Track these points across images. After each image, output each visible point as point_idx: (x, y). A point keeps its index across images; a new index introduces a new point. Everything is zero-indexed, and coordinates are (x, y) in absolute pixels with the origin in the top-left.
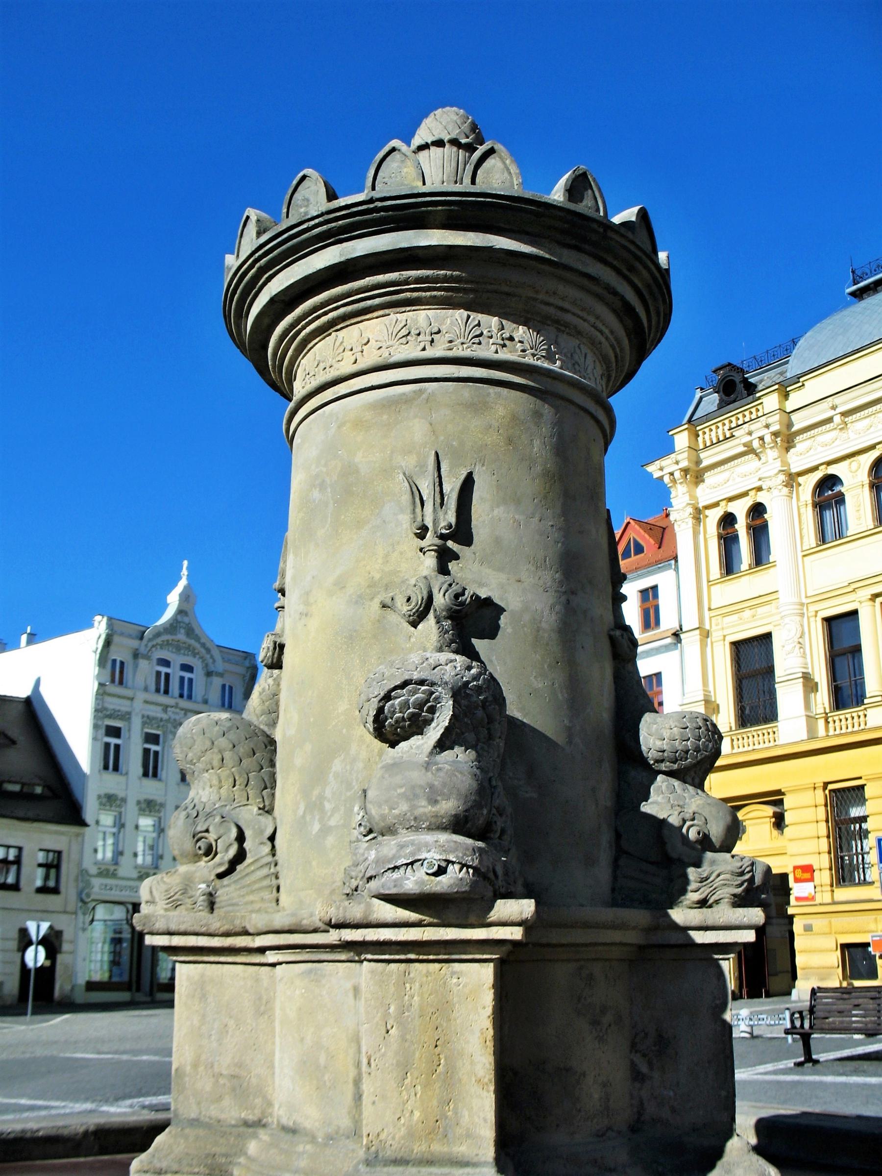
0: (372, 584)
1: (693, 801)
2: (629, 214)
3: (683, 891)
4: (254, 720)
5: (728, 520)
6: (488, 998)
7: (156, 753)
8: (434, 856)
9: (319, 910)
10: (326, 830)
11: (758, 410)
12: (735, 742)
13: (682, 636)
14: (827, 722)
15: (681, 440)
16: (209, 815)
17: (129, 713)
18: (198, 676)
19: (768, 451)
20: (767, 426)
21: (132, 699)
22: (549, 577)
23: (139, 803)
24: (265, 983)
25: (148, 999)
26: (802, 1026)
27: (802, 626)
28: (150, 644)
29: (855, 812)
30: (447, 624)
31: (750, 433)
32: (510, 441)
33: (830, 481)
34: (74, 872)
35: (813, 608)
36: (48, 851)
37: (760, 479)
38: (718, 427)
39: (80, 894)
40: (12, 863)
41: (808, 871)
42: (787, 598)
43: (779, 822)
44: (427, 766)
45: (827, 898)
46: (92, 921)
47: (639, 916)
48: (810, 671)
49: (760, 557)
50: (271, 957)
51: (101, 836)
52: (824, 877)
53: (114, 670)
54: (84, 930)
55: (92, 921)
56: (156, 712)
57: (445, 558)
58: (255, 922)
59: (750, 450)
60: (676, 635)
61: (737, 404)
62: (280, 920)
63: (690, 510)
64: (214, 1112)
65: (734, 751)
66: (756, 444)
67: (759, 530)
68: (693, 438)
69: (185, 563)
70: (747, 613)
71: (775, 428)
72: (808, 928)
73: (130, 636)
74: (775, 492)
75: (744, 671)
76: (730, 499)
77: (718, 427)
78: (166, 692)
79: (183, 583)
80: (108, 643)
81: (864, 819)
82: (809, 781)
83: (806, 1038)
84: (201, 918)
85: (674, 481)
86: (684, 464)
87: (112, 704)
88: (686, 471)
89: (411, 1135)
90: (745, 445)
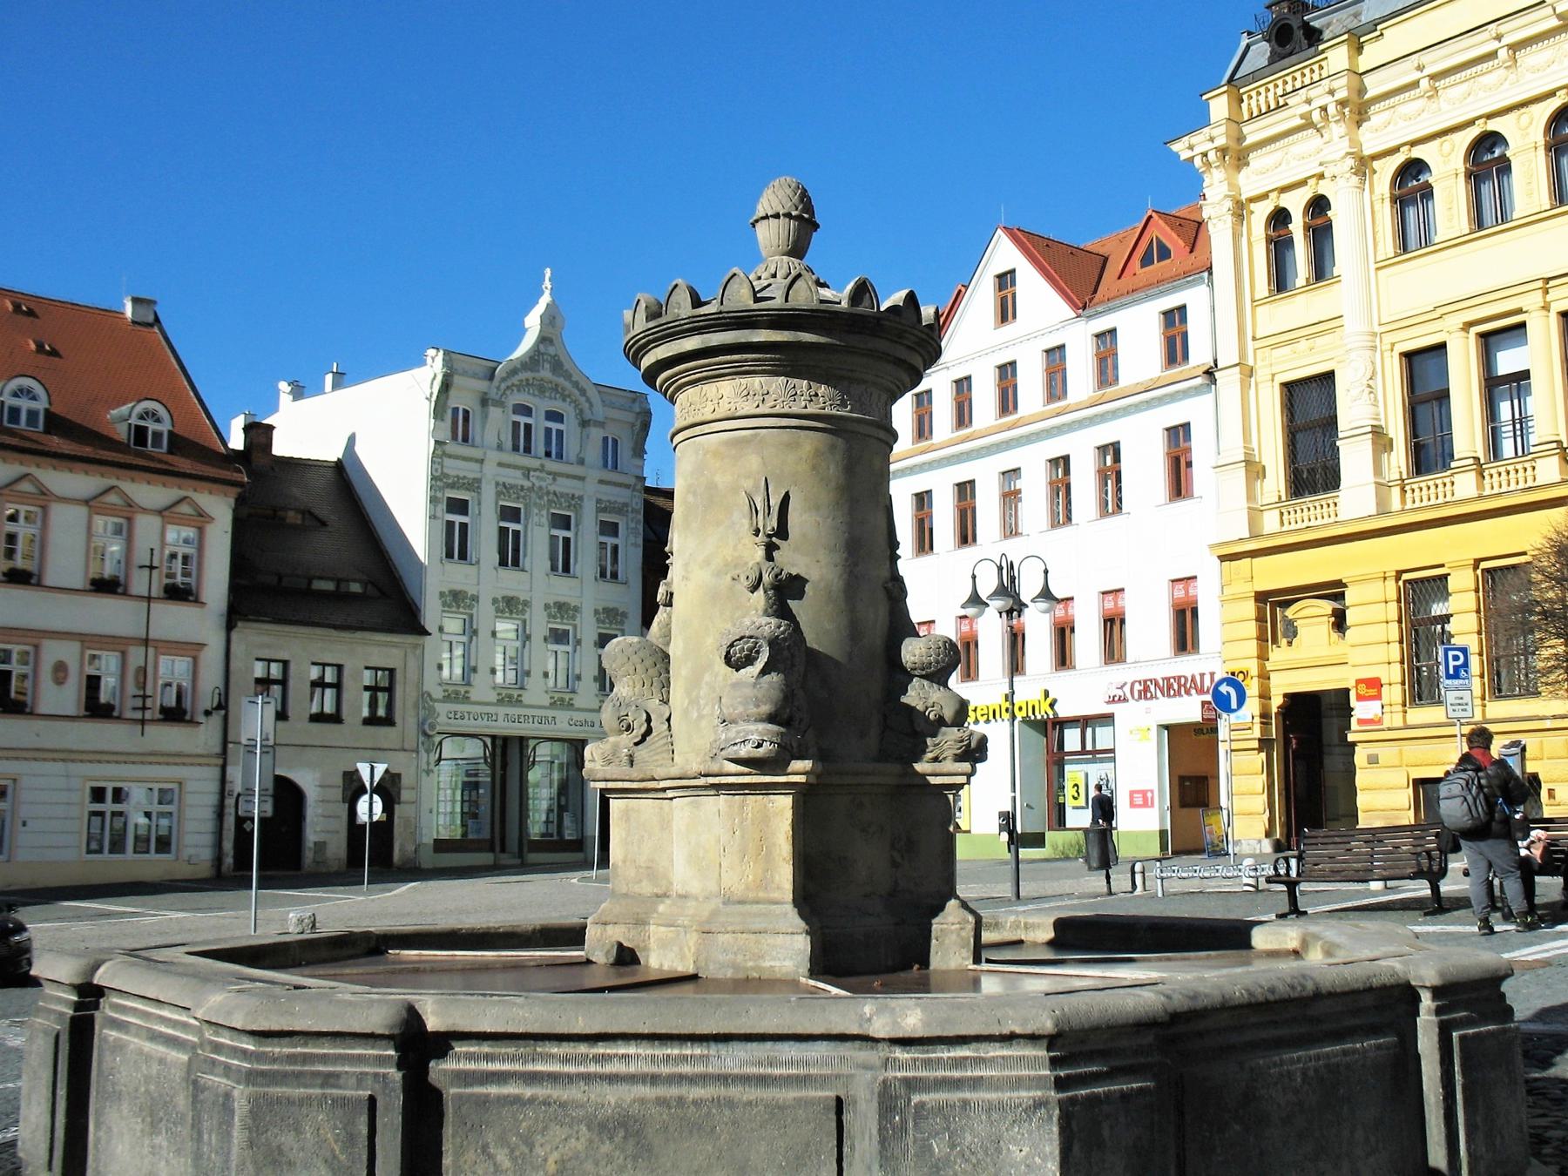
0: (726, 565)
1: (935, 694)
2: (898, 298)
3: (924, 752)
4: (654, 641)
5: (1280, 217)
6: (789, 814)
7: (516, 534)
8: (756, 737)
9: (695, 767)
10: (701, 717)
11: (1321, 68)
12: (1286, 517)
14: (1403, 491)
15: (1219, 107)
16: (628, 705)
17: (479, 481)
18: (569, 426)
19: (1333, 125)
20: (1332, 92)
21: (481, 461)
22: (839, 557)
23: (495, 601)
24: (667, 809)
25: (518, 861)
26: (1288, 874)
28: (503, 386)
29: (1437, 609)
30: (770, 593)
31: (1309, 102)
32: (814, 468)
34: (412, 695)
35: (1388, 339)
36: (377, 669)
38: (1268, 90)
39: (420, 725)
40: (330, 685)
41: (1375, 684)
42: (1355, 327)
43: (1339, 622)
44: (755, 685)
45: (1398, 721)
46: (440, 759)
47: (895, 768)
48: (1383, 423)
49: (1321, 270)
50: (670, 794)
51: (446, 646)
52: (1394, 693)
53: (455, 422)
54: (428, 772)
55: (440, 759)
56: (515, 477)
57: (770, 549)
58: (659, 772)
59: (1308, 124)
60: (1209, 373)
61: (1294, 58)
62: (674, 771)
63: (1229, 204)
64: (636, 889)
65: (1286, 528)
66: (1316, 117)
67: (1321, 234)
68: (1235, 105)
69: (548, 272)
70: (1304, 344)
71: (1342, 94)
72: (1373, 760)
73: (475, 376)
74: (1340, 182)
75: (1299, 421)
77: (1268, 90)
78: (528, 450)
79: (546, 299)
80: (446, 386)
81: (1446, 619)
82: (1377, 569)
83: (1292, 885)
84: (625, 770)
85: (1208, 165)
86: (1221, 141)
87: (454, 468)
88: (1223, 151)
89: (747, 888)
90: (1302, 116)
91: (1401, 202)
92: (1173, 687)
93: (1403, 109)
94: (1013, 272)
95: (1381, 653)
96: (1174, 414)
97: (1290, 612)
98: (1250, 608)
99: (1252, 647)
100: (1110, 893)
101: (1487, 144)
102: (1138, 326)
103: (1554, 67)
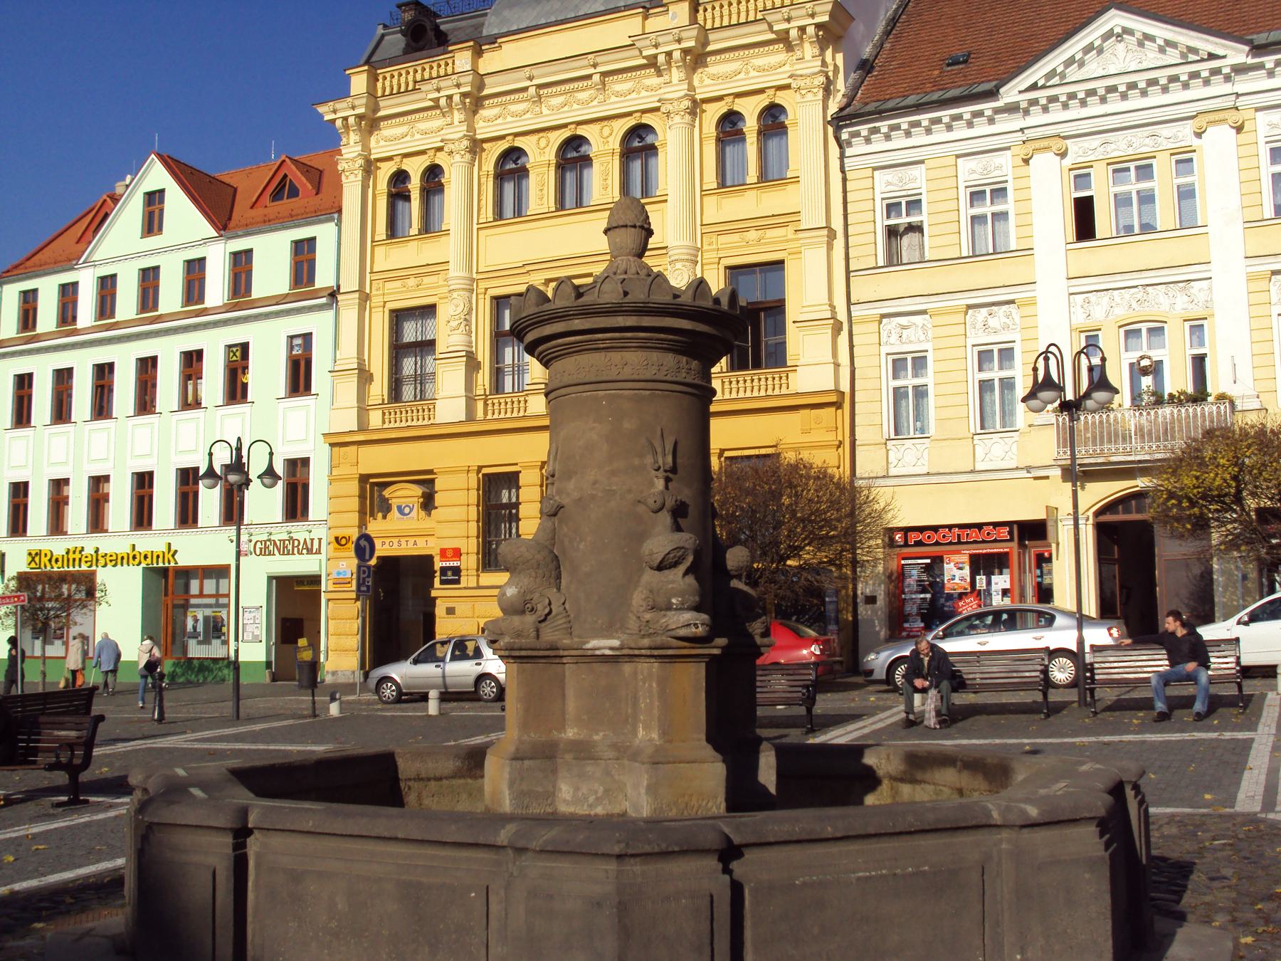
5: (400, 177)
12: (387, 416)
13: (339, 297)
14: (486, 405)
15: (359, 82)
27: (470, 302)
33: (514, 154)
35: (483, 285)
37: (790, 77)
63: (361, 162)
65: (386, 426)
66: (443, 102)
72: (451, 611)
74: (457, 158)
76: (738, 95)
85: (346, 127)
91: (501, 176)
92: (287, 548)
93: (513, 108)
94: (162, 191)
95: (460, 529)
96: (299, 324)
97: (386, 493)
98: (354, 487)
99: (354, 518)
100: (315, 716)
101: (575, 144)
102: (271, 254)
103: (634, 95)
